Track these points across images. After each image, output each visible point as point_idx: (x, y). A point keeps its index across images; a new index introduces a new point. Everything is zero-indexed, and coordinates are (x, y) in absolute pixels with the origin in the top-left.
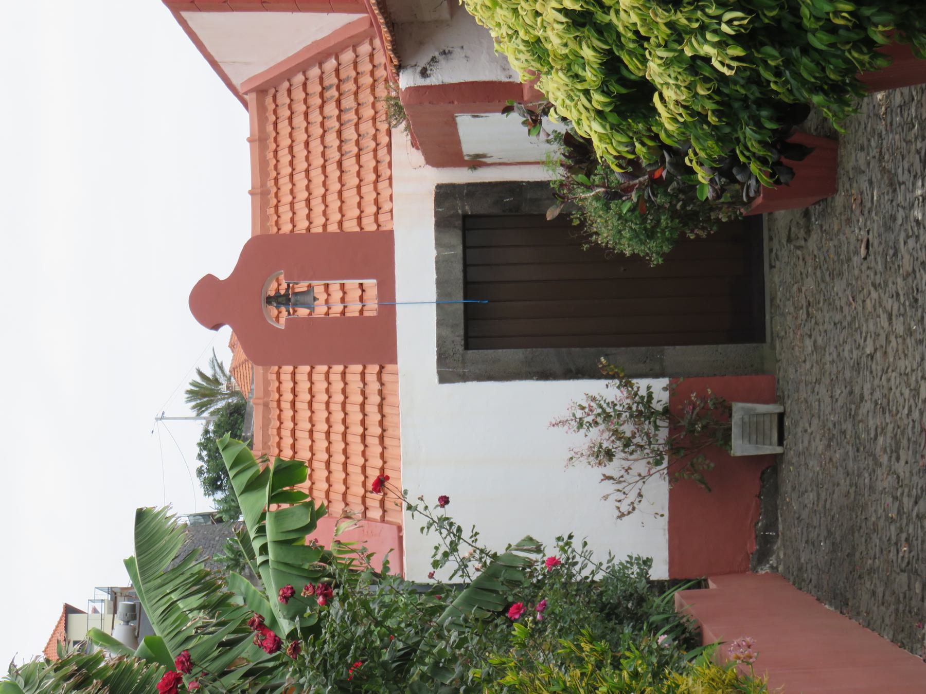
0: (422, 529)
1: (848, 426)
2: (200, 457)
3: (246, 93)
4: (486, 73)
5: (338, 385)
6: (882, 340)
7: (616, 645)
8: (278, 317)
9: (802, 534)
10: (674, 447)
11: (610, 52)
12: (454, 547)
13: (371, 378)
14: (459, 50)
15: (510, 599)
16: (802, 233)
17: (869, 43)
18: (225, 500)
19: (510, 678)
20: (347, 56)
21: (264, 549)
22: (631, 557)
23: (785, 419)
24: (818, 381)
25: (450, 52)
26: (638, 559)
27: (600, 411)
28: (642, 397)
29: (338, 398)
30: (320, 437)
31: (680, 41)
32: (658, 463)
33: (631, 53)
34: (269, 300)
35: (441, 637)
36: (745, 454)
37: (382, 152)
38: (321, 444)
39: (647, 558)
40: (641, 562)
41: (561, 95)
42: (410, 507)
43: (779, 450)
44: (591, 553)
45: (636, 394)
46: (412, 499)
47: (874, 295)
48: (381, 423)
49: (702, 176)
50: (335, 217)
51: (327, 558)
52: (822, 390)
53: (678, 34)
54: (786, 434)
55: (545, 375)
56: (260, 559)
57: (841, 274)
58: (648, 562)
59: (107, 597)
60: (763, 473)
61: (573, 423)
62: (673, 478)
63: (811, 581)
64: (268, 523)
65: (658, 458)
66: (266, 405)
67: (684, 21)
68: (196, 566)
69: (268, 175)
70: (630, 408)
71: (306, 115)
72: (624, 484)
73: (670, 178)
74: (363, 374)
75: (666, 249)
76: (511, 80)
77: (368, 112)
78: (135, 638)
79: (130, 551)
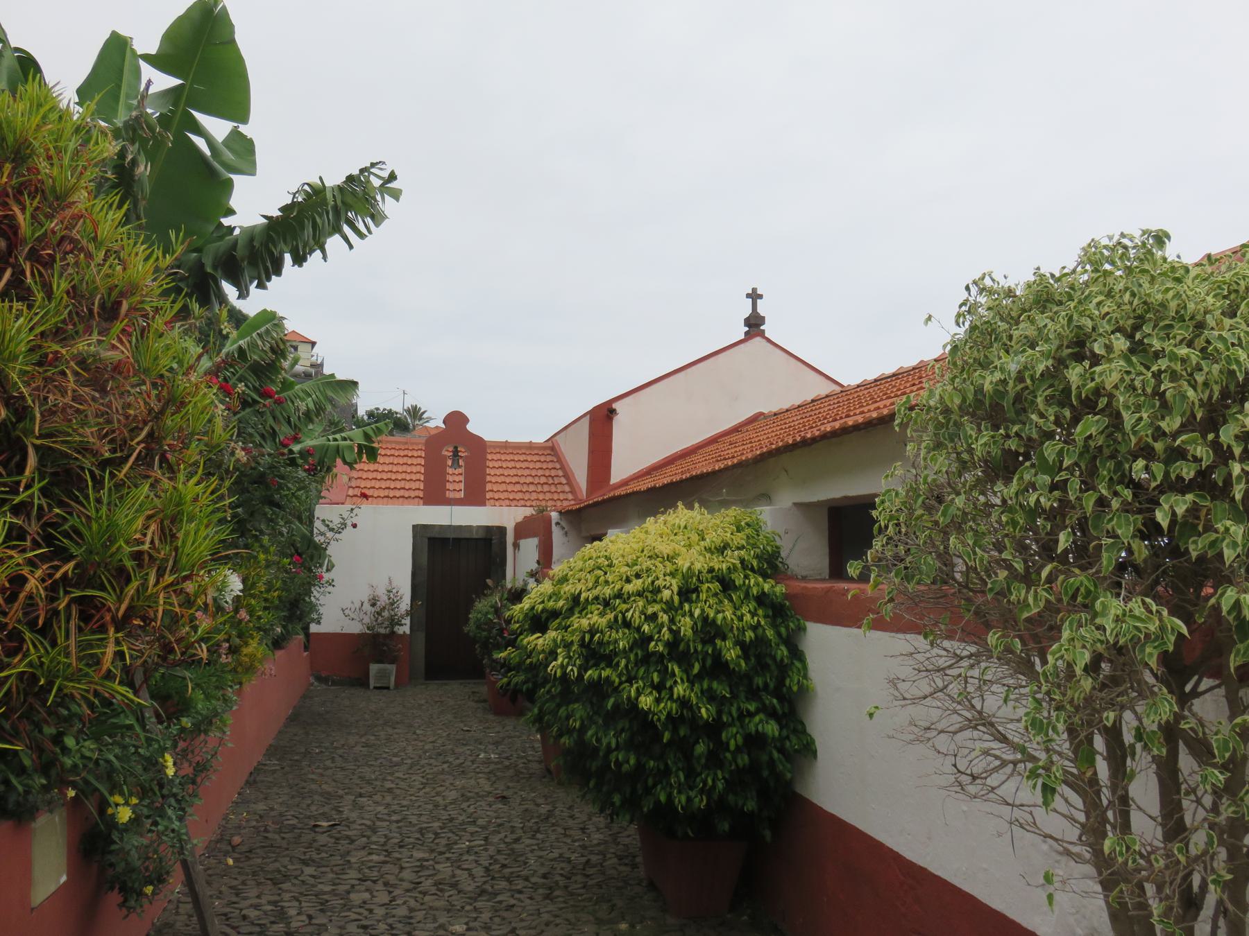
1: (381, 722)
7: (277, 608)
8: (447, 452)
11: (561, 614)
12: (332, 530)
16: (476, 699)
17: (560, 735)
19: (262, 556)
20: (567, 488)
24: (404, 706)
30: (390, 468)
31: (564, 647)
32: (368, 628)
33: (560, 624)
34: (456, 448)
35: (286, 523)
37: (522, 502)
38: (386, 468)
41: (542, 590)
42: (352, 509)
43: (371, 687)
47: (445, 734)
48: (395, 497)
49: (503, 655)
50: (493, 480)
51: (329, 469)
53: (568, 646)
56: (330, 437)
57: (455, 717)
58: (319, 623)
59: (319, 362)
64: (348, 442)
66: (406, 443)
68: (329, 408)
73: (503, 638)
75: (471, 634)
77: (541, 496)
78: (296, 376)
79: (339, 377)
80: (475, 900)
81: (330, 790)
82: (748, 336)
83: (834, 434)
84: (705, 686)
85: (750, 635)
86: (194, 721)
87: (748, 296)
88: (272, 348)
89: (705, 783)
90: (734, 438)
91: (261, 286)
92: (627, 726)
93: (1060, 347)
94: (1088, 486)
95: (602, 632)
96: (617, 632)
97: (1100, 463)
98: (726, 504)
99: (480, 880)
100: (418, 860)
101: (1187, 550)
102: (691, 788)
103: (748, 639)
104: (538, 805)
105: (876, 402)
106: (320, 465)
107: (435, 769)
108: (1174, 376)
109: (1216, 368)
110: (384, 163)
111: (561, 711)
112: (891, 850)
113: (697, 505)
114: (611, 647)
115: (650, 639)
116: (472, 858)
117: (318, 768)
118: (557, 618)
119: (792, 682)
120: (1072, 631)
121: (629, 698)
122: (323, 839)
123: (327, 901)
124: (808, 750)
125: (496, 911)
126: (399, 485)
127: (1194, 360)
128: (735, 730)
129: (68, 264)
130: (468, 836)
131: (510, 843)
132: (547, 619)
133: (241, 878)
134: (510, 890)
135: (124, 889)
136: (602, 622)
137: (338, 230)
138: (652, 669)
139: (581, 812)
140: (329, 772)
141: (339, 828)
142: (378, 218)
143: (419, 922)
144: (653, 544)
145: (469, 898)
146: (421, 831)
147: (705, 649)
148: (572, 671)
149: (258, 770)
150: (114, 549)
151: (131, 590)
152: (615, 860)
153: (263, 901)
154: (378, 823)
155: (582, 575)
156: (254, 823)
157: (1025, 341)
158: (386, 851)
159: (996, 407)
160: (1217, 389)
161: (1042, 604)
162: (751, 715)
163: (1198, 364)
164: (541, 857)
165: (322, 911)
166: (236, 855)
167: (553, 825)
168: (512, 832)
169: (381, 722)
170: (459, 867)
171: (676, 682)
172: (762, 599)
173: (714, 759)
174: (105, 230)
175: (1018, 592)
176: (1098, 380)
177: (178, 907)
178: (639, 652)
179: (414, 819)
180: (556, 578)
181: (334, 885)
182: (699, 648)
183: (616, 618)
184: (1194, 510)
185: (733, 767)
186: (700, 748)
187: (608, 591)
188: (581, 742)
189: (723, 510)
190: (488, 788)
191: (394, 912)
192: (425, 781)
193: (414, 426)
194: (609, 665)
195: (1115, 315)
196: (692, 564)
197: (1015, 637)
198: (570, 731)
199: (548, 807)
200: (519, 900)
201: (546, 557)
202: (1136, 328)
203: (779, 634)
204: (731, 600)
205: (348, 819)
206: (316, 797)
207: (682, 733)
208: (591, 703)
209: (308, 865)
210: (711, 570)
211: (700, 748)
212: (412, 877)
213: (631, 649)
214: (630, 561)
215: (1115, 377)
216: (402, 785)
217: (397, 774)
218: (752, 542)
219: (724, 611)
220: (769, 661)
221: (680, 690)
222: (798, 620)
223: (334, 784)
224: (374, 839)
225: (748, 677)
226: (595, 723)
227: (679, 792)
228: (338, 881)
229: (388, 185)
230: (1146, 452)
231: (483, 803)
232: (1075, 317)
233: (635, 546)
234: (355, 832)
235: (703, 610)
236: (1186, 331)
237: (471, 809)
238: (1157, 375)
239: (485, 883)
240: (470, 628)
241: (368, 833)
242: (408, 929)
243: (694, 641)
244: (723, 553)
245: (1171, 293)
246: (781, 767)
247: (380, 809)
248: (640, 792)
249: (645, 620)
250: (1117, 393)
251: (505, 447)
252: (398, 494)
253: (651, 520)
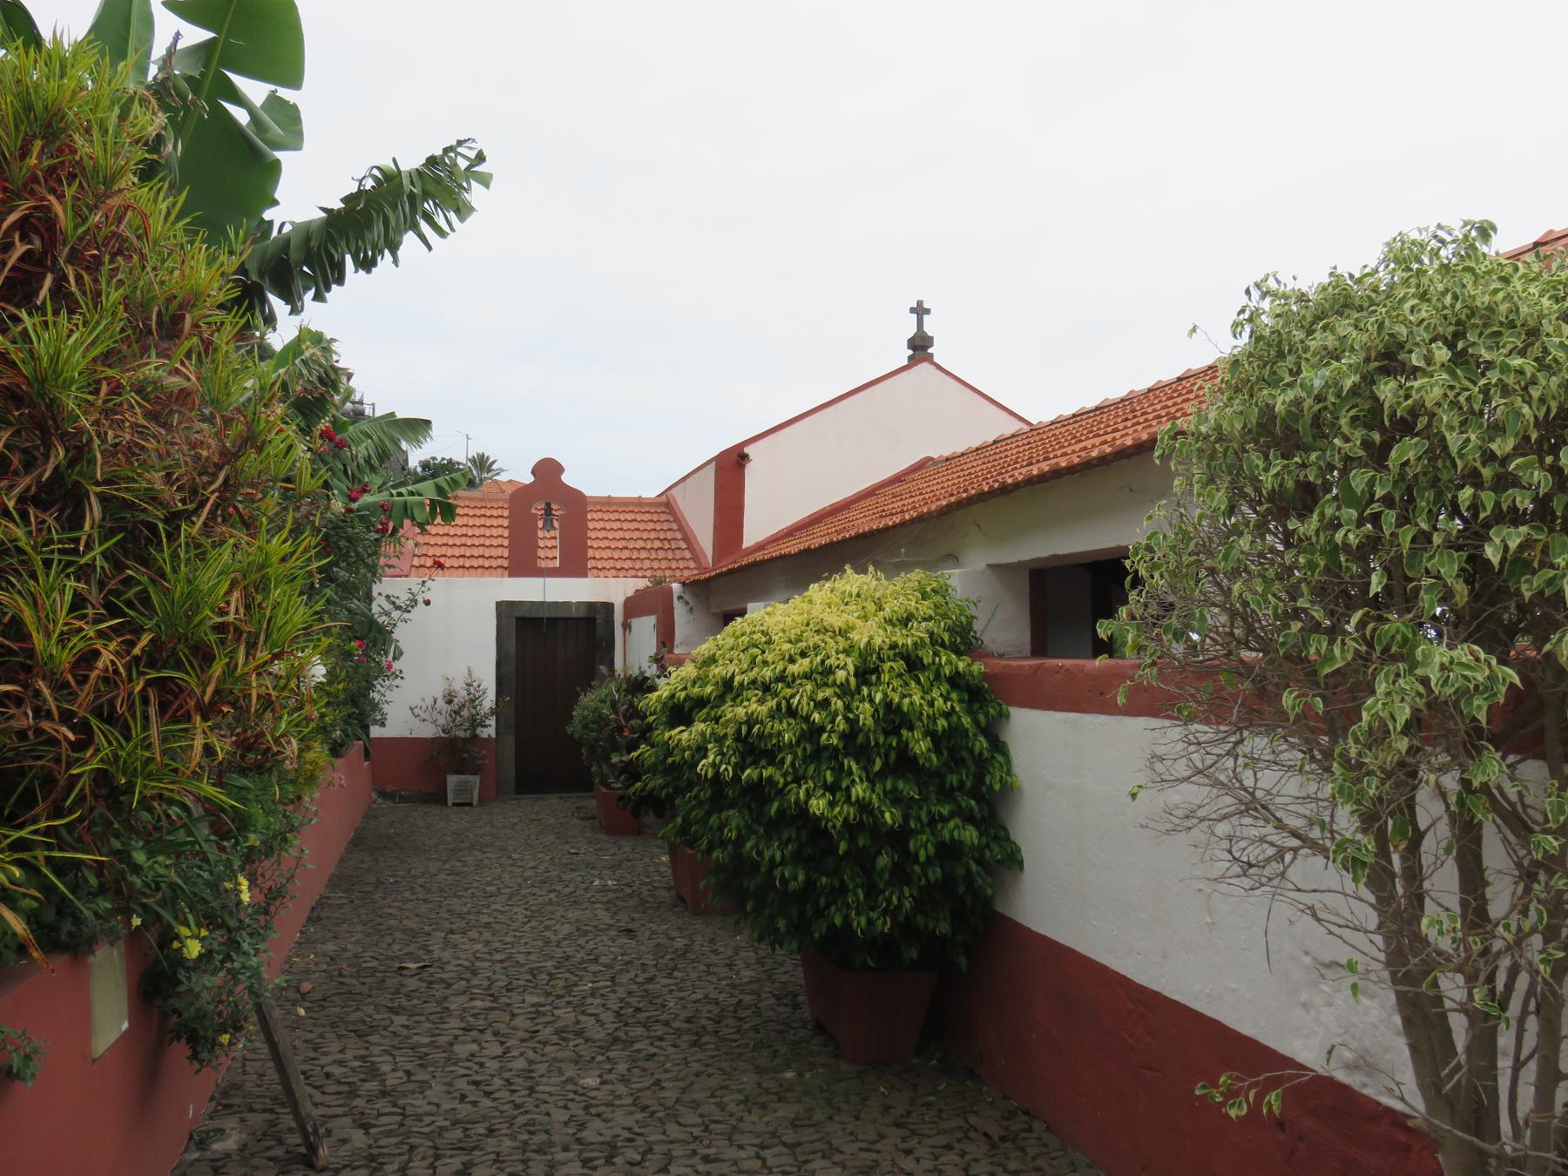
1: (466, 844)
2: (443, 459)
4: (680, 632)
5: (495, 542)
6: (520, 864)
8: (537, 509)
10: (453, 741)
12: (398, 608)
13: (500, 562)
16: (582, 815)
18: (416, 472)
20: (688, 555)
21: (400, 494)
29: (488, 542)
32: (444, 731)
33: (708, 714)
34: (548, 504)
37: (633, 573)
41: (683, 674)
43: (450, 803)
46: (428, 584)
47: (547, 858)
48: (472, 567)
52: (488, 829)
53: (720, 740)
56: (394, 492)
58: (383, 725)
62: (433, 740)
64: (416, 498)
66: (482, 500)
67: (727, 743)
71: (654, 530)
74: (502, 557)
77: (656, 565)
79: (399, 416)
80: (608, 1049)
81: (414, 926)
82: (913, 361)
83: (1043, 478)
84: (889, 785)
85: (942, 723)
86: (264, 838)
87: (912, 310)
88: (320, 378)
89: (889, 901)
90: (897, 489)
91: (319, 297)
92: (794, 835)
93: (1367, 360)
94: (1403, 520)
95: (762, 722)
96: (781, 722)
97: (1418, 491)
98: (907, 567)
99: (611, 1027)
100: (533, 1005)
101: (1518, 589)
102: (873, 909)
103: (940, 728)
104: (673, 939)
105: (1063, 447)
106: (388, 521)
107: (540, 899)
108: (1505, 390)
109: (1555, 380)
110: (474, 140)
111: (712, 820)
112: (1118, 974)
113: (871, 568)
114: (774, 741)
115: (822, 729)
116: (598, 1001)
117: (395, 900)
118: (704, 707)
119: (994, 780)
120: (1387, 682)
121: (797, 801)
122: (412, 984)
123: (427, 1055)
124: (1013, 860)
125: (634, 1061)
126: (476, 552)
127: (1529, 371)
128: (924, 838)
129: (117, 269)
130: (590, 977)
131: (643, 984)
132: (691, 710)
133: (318, 1030)
134: (648, 1037)
135: (194, 1039)
136: (763, 710)
137: (415, 227)
138: (824, 767)
139: (725, 946)
140: (409, 905)
141: (431, 970)
142: (463, 210)
143: (542, 1076)
144: (821, 616)
145: (600, 1047)
146: (531, 971)
147: (888, 741)
148: (727, 770)
149: (321, 903)
150: (197, 619)
151: (217, 669)
152: (772, 1001)
153: (349, 1055)
154: (478, 964)
155: (735, 654)
156: (325, 967)
157: (1324, 353)
158: (492, 995)
159: (1290, 431)
160: (1554, 405)
161: (1349, 657)
162: (945, 820)
163: (1533, 375)
164: (682, 999)
165: (422, 1066)
166: (307, 1004)
167: (693, 961)
168: (644, 971)
169: (466, 844)
170: (583, 1013)
171: (853, 782)
172: (956, 681)
173: (900, 874)
174: (157, 225)
175: (1317, 646)
176: (1415, 396)
177: (244, 1065)
178: (808, 747)
179: (521, 958)
180: (700, 660)
181: (432, 1035)
182: (881, 741)
183: (779, 705)
184: (1526, 544)
185: (923, 882)
186: (883, 861)
187: (768, 673)
188: (737, 856)
189: (903, 574)
190: (607, 920)
191: (510, 1065)
192: (529, 913)
193: (481, 480)
194: (771, 763)
195: (1433, 321)
196: (871, 638)
197: (1314, 696)
198: (723, 844)
199: (685, 941)
200: (661, 1048)
201: (666, 636)
202: (1458, 335)
203: (976, 722)
204: (918, 682)
205: (440, 959)
206: (398, 935)
207: (861, 843)
208: (750, 809)
209: (398, 1014)
210: (893, 646)
211: (883, 861)
212: (528, 1024)
213: (798, 743)
214: (793, 636)
215: (1437, 392)
216: (502, 918)
217: (494, 907)
218: (941, 612)
219: (910, 696)
220: (964, 754)
221: (859, 791)
222: (1000, 705)
223: (418, 919)
224: (475, 982)
225: (938, 775)
226: (756, 833)
227: (858, 914)
228: (437, 1032)
229: (476, 169)
230: (1474, 478)
231: (605, 938)
232: (1387, 323)
233: (798, 619)
234: (451, 975)
235: (885, 695)
236: (1518, 339)
237: (591, 945)
238: (1485, 391)
239: (617, 1029)
240: (575, 728)
241: (468, 975)
242: (529, 1083)
243: (875, 732)
244: (906, 626)
245: (1500, 295)
246: (980, 882)
247: (479, 946)
248: (810, 914)
249: (815, 707)
250: (1439, 411)
251: (609, 504)
252: (475, 563)
253: (814, 587)
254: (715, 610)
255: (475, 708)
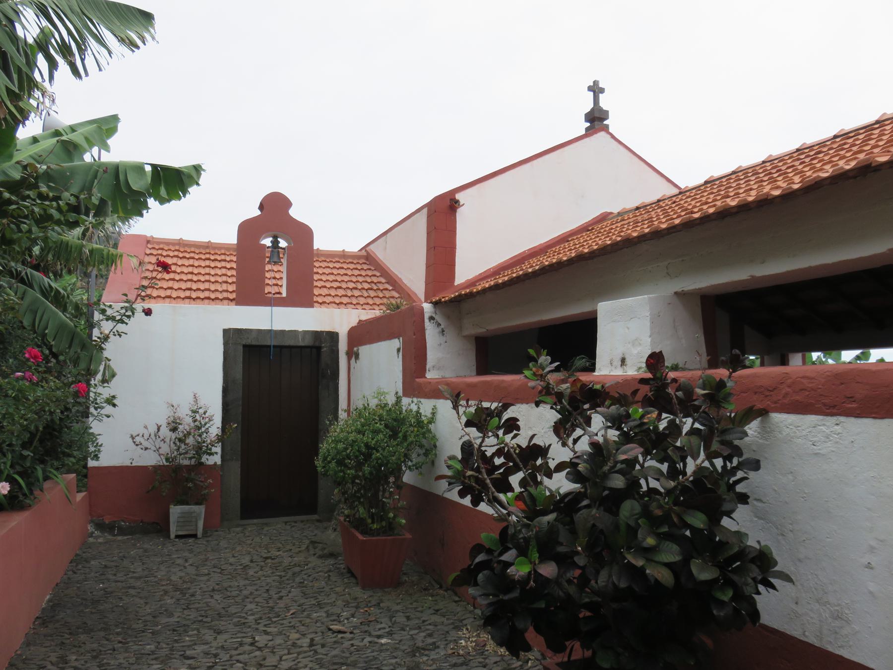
0: (126, 295)
3: (366, 251)
9: (113, 561)
10: (178, 469)
14: (444, 341)
15: (61, 358)
22: (101, 445)
23: (193, 539)
25: (443, 335)
26: (99, 451)
27: (203, 423)
28: (210, 449)
32: (167, 460)
36: (171, 515)
39: (99, 457)
40: (97, 453)
43: (172, 536)
44: (100, 421)
45: (213, 446)
54: (183, 540)
55: (225, 391)
60: (157, 524)
61: (196, 407)
62: (156, 468)
63: (75, 573)
65: (171, 460)
69: (327, 258)
70: (204, 442)
72: (154, 438)
76: (427, 371)
82: (589, 132)
87: (590, 89)
254: (466, 333)
255: (200, 436)
